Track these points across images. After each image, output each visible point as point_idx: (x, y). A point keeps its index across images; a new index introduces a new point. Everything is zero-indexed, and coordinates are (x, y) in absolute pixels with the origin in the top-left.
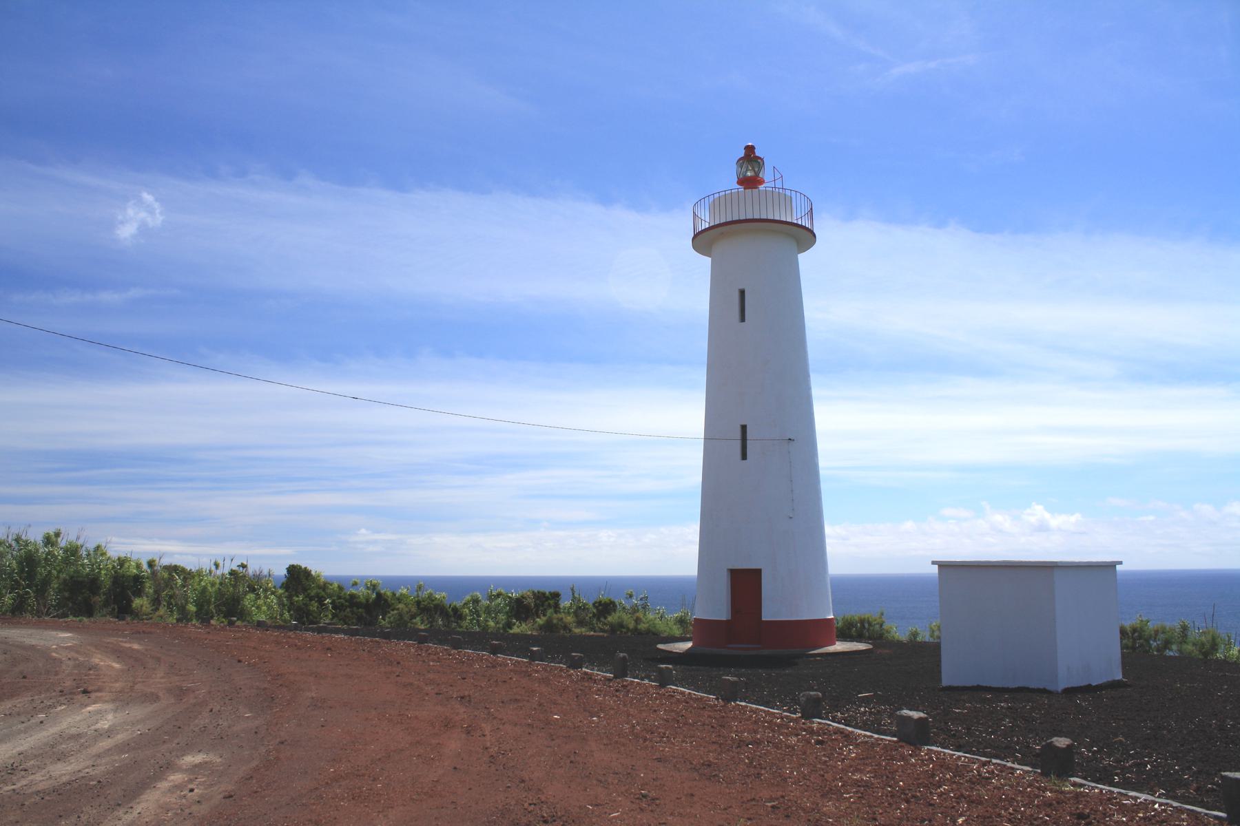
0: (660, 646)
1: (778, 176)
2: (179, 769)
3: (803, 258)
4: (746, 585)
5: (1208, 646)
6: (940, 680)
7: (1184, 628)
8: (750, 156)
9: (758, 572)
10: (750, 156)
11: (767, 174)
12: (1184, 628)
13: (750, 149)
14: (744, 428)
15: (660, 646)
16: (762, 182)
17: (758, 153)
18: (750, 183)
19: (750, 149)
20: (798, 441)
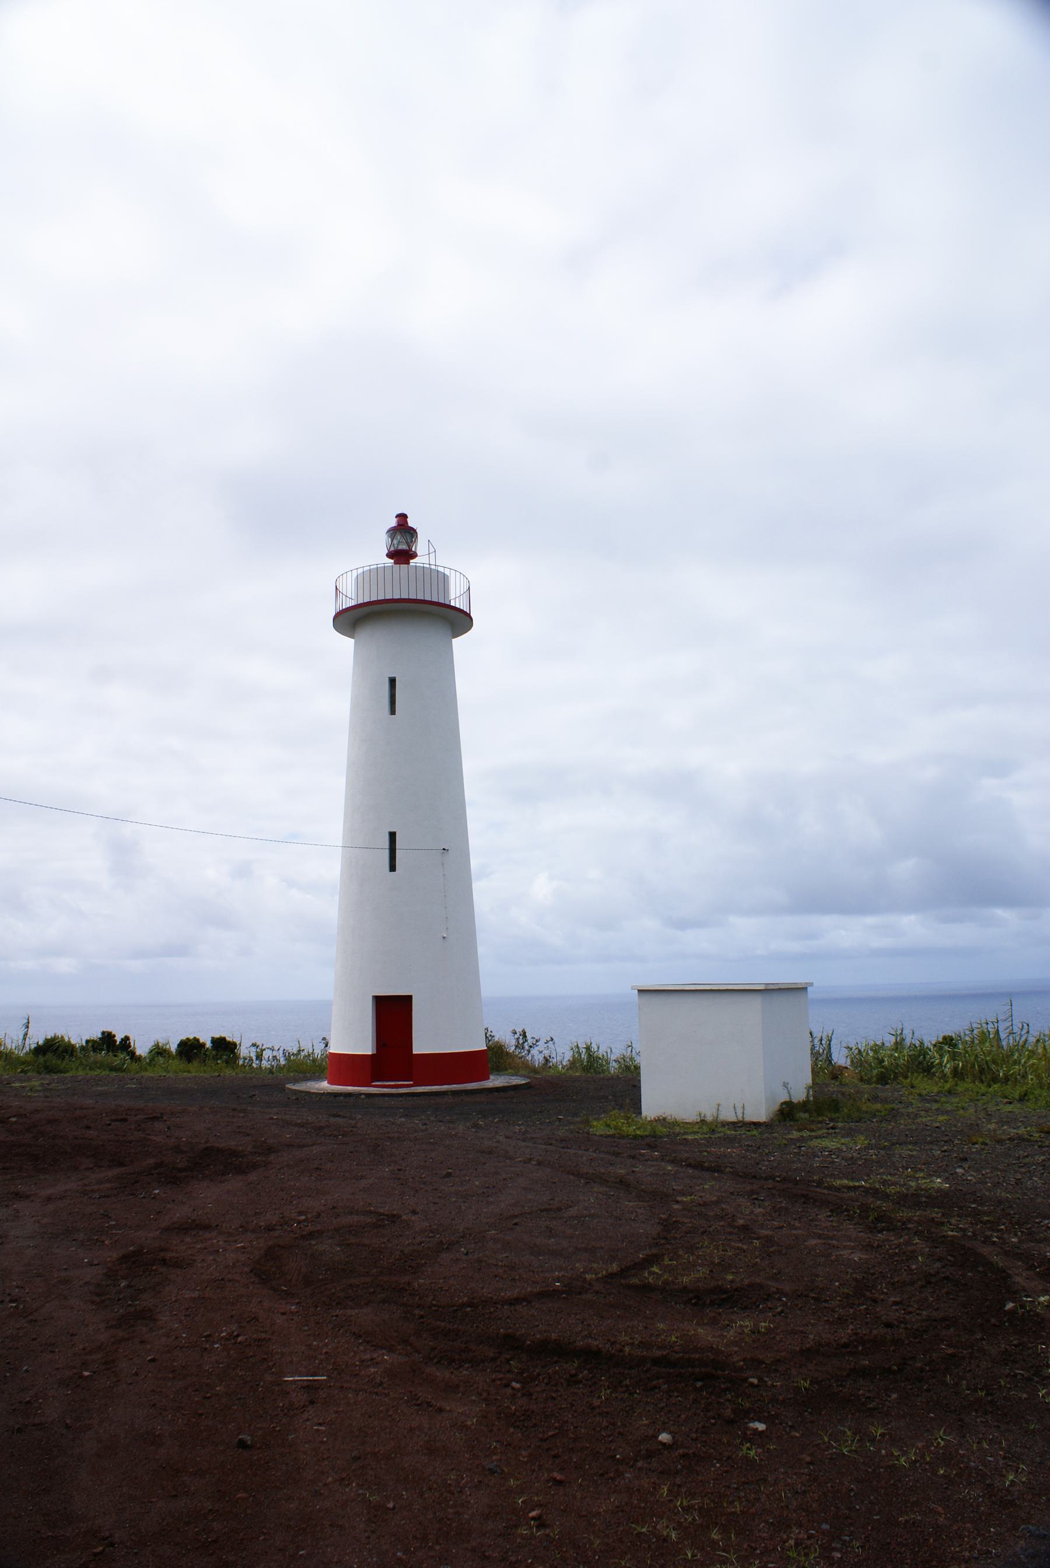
0: (288, 1086)
1: (431, 550)
2: (948, 1062)
3: (456, 642)
4: (393, 1014)
5: (168, 1255)
6: (638, 1110)
7: (351, 619)
8: (403, 528)
9: (408, 999)
10: (403, 528)
11: (421, 547)
12: (351, 619)
13: (402, 517)
14: (392, 836)
15: (288, 1086)
16: (414, 555)
17: (411, 523)
18: (402, 556)
19: (402, 517)
20: (451, 853)
